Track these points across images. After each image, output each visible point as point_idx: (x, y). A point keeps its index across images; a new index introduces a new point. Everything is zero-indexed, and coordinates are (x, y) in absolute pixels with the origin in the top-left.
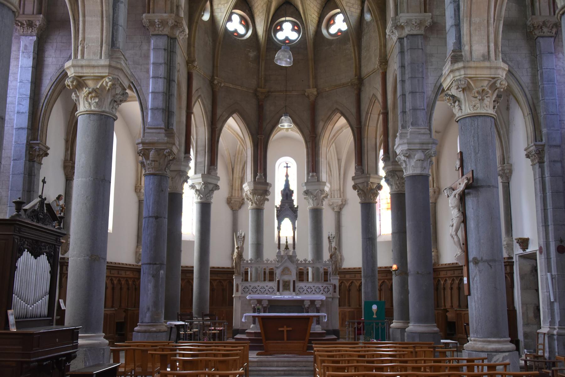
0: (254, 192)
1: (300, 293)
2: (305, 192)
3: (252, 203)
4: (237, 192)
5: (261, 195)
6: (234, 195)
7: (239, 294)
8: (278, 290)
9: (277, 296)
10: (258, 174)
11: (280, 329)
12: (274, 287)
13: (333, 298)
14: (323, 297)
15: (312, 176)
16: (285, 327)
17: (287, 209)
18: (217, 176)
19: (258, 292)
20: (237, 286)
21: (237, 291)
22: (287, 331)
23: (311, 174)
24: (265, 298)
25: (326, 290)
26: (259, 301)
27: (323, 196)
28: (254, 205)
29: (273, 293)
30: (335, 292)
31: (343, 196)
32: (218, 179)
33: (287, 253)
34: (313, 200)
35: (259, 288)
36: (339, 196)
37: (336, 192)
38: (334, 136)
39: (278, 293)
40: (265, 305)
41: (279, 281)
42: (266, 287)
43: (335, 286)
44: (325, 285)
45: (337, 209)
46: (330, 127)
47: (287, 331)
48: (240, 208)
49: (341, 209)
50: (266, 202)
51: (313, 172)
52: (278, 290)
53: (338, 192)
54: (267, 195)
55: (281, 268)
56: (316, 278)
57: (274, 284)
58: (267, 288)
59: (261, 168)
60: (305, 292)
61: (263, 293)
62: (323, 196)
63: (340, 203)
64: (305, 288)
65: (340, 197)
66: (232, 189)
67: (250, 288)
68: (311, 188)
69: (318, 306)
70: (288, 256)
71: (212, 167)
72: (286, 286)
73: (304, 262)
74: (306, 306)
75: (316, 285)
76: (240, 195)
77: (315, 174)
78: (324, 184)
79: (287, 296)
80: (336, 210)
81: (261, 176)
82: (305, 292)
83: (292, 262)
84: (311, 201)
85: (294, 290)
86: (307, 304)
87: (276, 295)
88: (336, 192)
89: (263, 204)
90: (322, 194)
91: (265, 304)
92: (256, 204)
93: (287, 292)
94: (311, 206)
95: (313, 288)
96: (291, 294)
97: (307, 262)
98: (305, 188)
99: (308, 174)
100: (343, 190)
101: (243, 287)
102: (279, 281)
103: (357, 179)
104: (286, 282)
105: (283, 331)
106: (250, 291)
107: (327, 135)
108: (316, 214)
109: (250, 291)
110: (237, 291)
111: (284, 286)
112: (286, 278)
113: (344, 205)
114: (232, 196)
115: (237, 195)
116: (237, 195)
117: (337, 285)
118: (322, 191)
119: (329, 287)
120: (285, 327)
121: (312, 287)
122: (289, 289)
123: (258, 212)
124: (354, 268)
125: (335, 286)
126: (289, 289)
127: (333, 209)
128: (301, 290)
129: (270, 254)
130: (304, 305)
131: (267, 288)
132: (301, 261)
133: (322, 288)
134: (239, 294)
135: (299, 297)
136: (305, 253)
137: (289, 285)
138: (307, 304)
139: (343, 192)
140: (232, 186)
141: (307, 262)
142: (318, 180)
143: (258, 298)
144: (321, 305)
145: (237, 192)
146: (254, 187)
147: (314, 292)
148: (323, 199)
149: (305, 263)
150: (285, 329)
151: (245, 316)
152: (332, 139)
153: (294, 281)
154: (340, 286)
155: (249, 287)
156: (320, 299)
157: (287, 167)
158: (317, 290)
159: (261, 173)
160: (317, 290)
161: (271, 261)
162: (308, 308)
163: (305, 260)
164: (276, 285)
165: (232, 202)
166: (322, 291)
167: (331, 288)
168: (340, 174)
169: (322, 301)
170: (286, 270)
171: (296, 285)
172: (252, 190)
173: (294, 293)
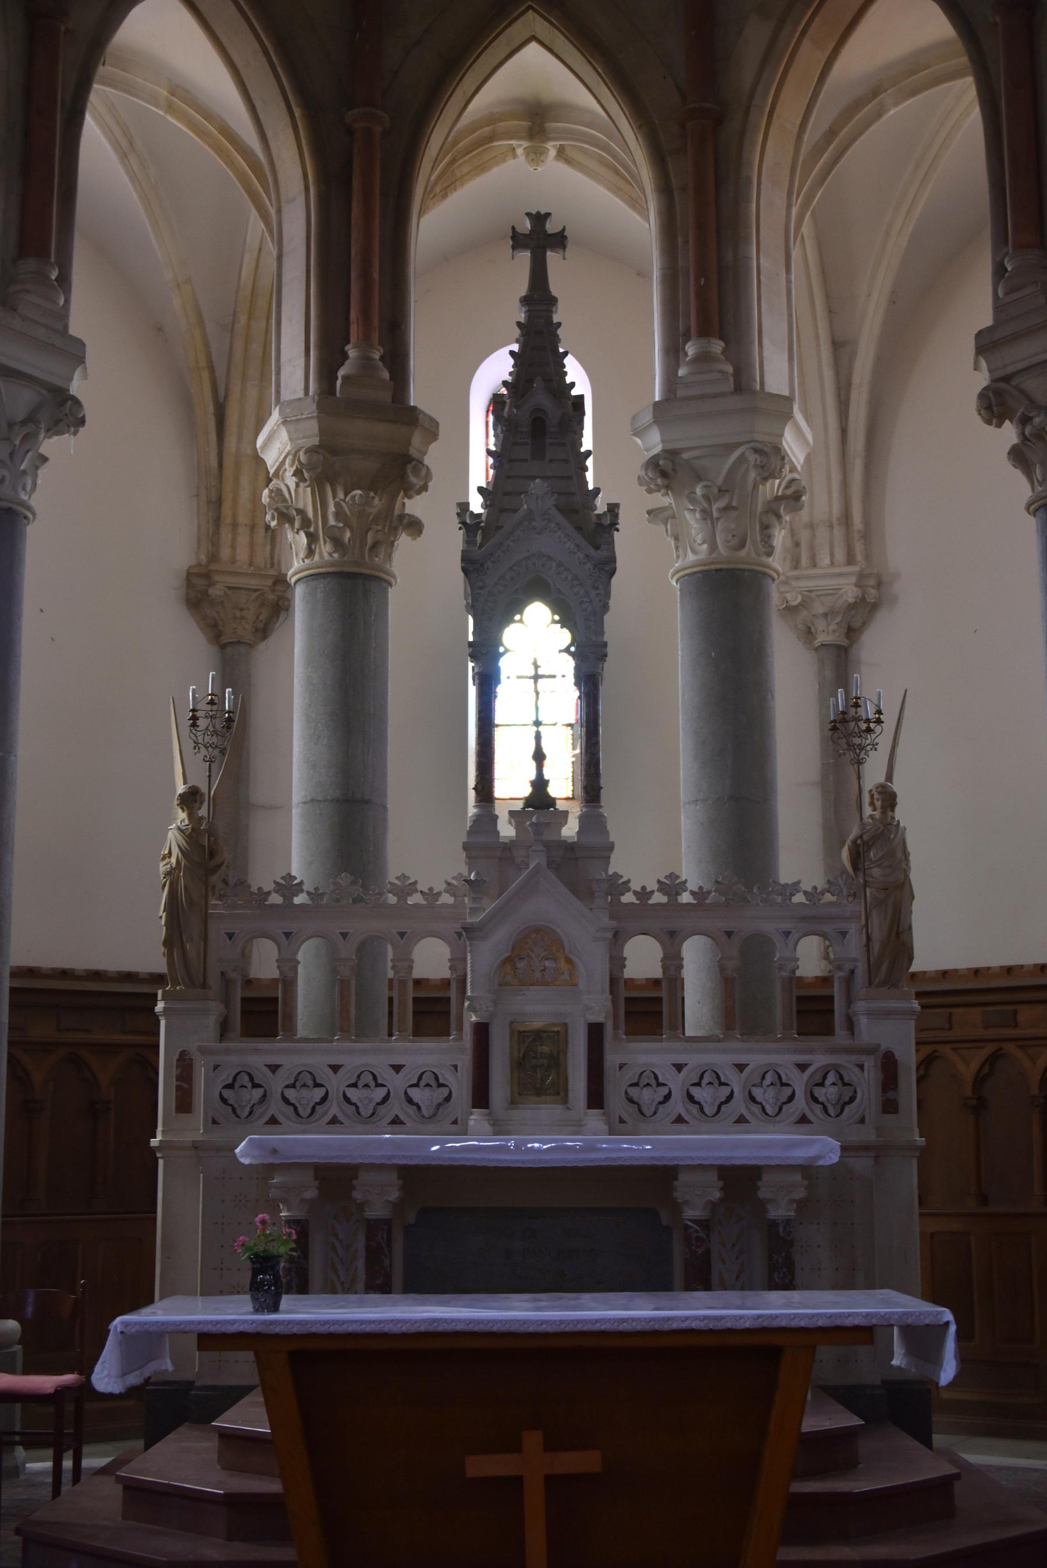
0: (323, 465)
1: (641, 1116)
2: (653, 463)
3: (312, 538)
4: (243, 539)
5: (372, 486)
6: (225, 553)
7: (195, 1128)
8: (481, 1098)
9: (474, 1142)
10: (352, 352)
11: (481, 1466)
12: (447, 1077)
13: (878, 1151)
14: (823, 1148)
15: (703, 358)
16: (533, 1440)
17: (543, 536)
18: (64, 332)
19: (333, 1109)
20: (185, 1067)
21: (184, 1103)
22: (550, 1480)
23: (691, 349)
24: (376, 1155)
25: (829, 1092)
26: (336, 1179)
27: (774, 487)
28: (325, 549)
29: (438, 1116)
30: (890, 1106)
31: (867, 557)
32: (74, 353)
33: (550, 855)
34: (706, 514)
35: (336, 1084)
36: (840, 555)
37: (822, 533)
38: (831, 134)
39: (476, 1117)
40: (377, 1211)
41: (482, 1031)
42: (387, 1076)
43: (889, 1065)
44: (820, 1060)
45: (827, 634)
46: (809, 56)
47: (550, 1480)
48: (263, 632)
49: (852, 633)
50: (404, 540)
51: (705, 331)
52: (481, 1098)
53: (838, 533)
54: (410, 491)
55: (500, 938)
56: (742, 1007)
57: (446, 1056)
58: (397, 1083)
59: (366, 314)
60: (678, 1105)
61: (369, 1119)
62: (774, 487)
63: (850, 593)
64: (677, 1083)
65: (850, 560)
66: (217, 521)
67: (277, 1084)
68: (693, 437)
69: (779, 1212)
70: (549, 846)
71: (31, 264)
72: (538, 1066)
73: (658, 898)
74: (693, 1213)
75: (757, 1059)
76: (262, 557)
77: (717, 346)
78: (781, 409)
79: (543, 1139)
80: (822, 638)
81: (366, 361)
82: (678, 1105)
83: (582, 889)
84: (693, 522)
85: (596, 1099)
86: (696, 1202)
87: (464, 1132)
88: (822, 533)
89: (385, 544)
90: (767, 473)
91: (379, 1199)
92: (337, 543)
93: (548, 1111)
94: (696, 554)
95: (736, 1082)
96: (577, 1127)
97: (685, 898)
98: (654, 442)
99: (673, 351)
100: (866, 522)
101: (225, 1077)
102: (482, 1031)
103: (1015, 338)
104: (538, 1035)
105: (516, 1483)
106: (275, 1107)
107: (789, 110)
108: (729, 603)
109: (275, 1107)
110: (184, 1103)
111: (519, 1065)
112: (536, 1007)
113: (874, 607)
114: (214, 557)
115: (242, 555)
116: (242, 555)
117: (908, 1058)
118: (770, 458)
119: (852, 1075)
120: (533, 1440)
121: (730, 1075)
122: (560, 1092)
123: (355, 591)
124: (944, 974)
125: (889, 1065)
126: (560, 1092)
127: (808, 634)
128: (647, 1096)
129: (422, 852)
130: (676, 1208)
131: (397, 1083)
132: (644, 894)
133: (799, 1082)
134: (195, 1128)
135: (640, 1147)
136: (665, 842)
137: (557, 1062)
138: (696, 1202)
139: (866, 536)
140: (219, 502)
141: (685, 898)
142: (743, 381)
143: (324, 1156)
144: (802, 1205)
145: (243, 539)
146: (322, 432)
147: (739, 1105)
148: (773, 509)
149: (673, 905)
150: (533, 1462)
151: (127, 1338)
152: (818, 150)
153: (595, 1032)
154: (926, 1064)
155: (262, 1074)
156: (800, 1155)
157: (536, 677)
158: (766, 1095)
159: (366, 340)
160: (766, 1095)
161: (431, 895)
162: (705, 1225)
163: (672, 886)
164: (465, 1061)
165: (215, 592)
166: (801, 1102)
167: (867, 1082)
168: (844, 431)
169: (807, 1170)
170: (534, 954)
171: (612, 1058)
172: (311, 451)
173: (594, 1119)
